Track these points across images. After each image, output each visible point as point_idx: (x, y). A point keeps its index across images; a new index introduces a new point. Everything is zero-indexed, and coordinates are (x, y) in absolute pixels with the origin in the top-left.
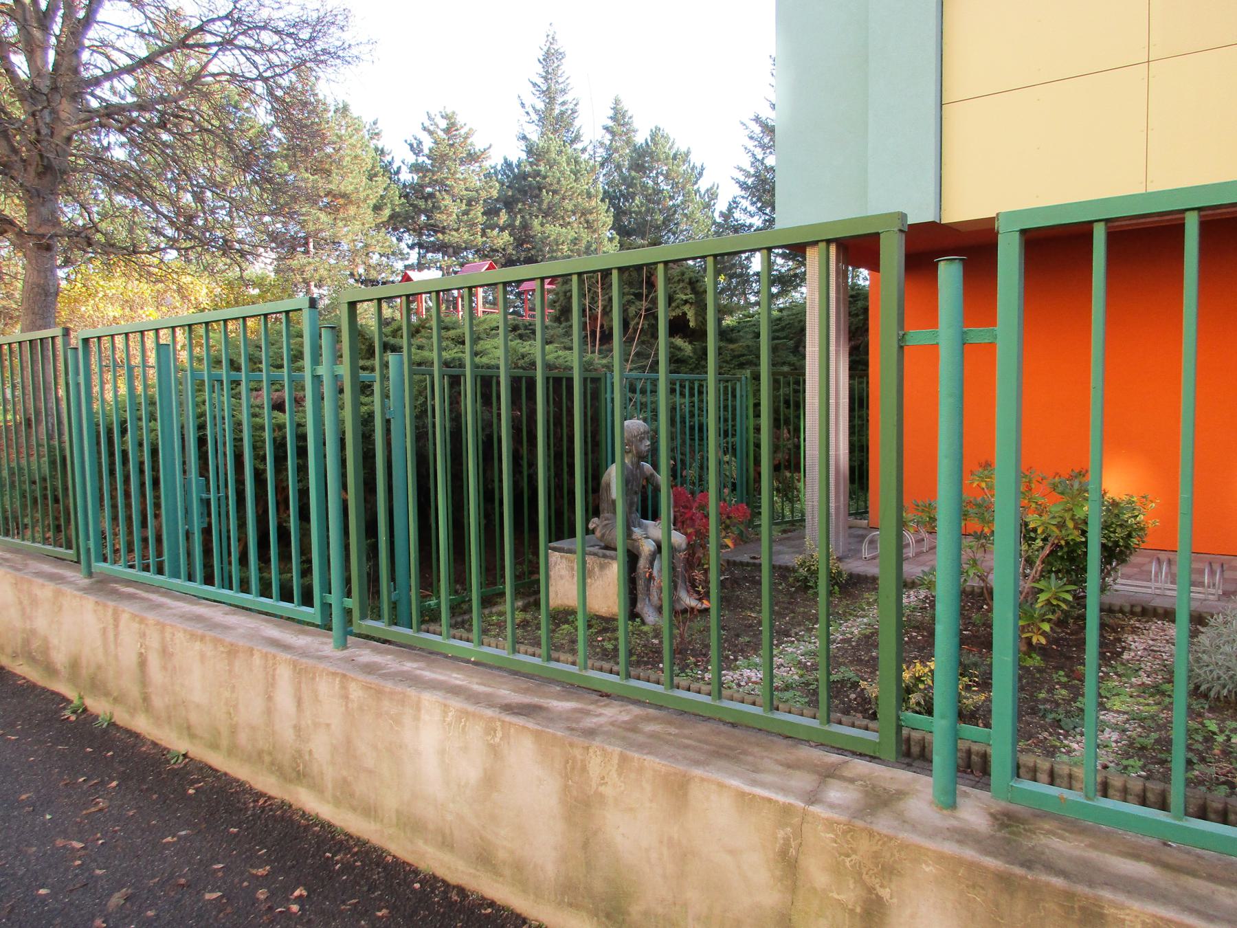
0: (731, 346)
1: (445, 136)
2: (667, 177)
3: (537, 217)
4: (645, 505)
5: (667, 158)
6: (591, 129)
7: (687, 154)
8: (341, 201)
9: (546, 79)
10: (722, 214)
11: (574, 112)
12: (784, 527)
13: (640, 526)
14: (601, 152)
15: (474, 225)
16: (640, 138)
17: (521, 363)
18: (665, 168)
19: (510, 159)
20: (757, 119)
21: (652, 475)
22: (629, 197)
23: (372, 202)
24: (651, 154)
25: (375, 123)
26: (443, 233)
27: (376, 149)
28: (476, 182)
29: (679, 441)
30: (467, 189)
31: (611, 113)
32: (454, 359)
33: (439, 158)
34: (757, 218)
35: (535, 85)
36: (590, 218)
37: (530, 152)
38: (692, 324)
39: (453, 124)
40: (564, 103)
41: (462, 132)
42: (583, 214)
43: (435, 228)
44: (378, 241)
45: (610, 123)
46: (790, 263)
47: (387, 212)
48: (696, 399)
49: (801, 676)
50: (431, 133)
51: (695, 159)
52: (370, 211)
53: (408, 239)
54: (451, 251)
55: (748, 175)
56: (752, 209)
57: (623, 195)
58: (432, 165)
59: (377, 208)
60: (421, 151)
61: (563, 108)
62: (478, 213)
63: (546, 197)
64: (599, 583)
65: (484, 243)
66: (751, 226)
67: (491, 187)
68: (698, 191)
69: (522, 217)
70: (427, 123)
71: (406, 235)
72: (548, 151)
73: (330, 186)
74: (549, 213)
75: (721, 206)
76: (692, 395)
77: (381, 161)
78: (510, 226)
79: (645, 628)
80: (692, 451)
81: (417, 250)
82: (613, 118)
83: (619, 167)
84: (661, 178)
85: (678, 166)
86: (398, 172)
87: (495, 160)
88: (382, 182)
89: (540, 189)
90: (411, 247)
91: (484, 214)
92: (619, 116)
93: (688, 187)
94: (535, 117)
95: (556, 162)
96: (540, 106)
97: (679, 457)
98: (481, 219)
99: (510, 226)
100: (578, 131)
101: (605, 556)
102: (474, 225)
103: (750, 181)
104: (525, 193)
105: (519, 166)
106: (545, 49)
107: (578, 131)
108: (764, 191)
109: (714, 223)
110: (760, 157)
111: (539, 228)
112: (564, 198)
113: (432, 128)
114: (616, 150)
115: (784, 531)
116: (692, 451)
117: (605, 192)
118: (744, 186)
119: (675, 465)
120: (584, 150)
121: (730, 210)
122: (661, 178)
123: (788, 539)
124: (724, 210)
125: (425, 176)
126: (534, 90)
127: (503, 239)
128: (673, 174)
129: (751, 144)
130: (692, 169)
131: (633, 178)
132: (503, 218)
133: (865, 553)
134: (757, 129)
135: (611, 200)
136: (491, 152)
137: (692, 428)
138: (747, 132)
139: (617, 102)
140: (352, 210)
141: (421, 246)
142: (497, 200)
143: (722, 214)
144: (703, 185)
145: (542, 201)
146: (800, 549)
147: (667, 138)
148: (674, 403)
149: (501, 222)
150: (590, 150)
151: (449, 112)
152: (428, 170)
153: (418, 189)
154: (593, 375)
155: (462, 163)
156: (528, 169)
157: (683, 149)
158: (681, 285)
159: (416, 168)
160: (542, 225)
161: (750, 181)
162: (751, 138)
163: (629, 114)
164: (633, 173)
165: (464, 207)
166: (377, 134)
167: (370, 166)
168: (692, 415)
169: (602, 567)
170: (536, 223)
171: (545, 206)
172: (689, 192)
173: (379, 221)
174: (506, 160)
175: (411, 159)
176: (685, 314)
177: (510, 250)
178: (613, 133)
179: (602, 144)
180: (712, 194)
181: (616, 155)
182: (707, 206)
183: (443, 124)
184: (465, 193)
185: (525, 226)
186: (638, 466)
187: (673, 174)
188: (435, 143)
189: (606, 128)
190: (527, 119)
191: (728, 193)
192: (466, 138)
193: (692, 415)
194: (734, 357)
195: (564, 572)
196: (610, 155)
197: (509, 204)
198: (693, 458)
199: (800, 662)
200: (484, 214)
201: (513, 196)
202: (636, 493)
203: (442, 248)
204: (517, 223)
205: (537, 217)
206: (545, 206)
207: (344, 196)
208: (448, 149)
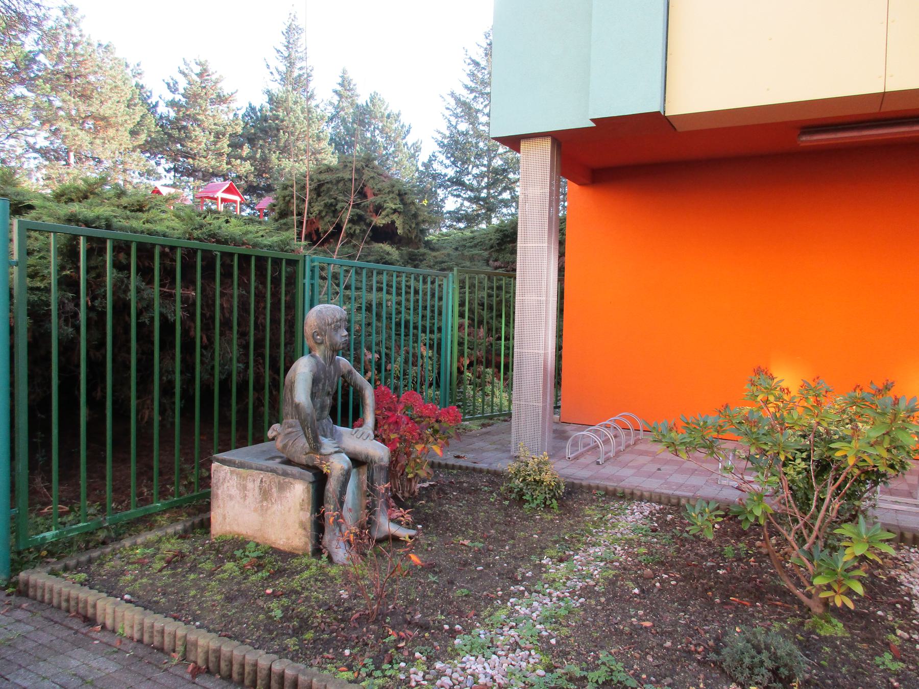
0: (434, 254)
1: (198, 80)
2: (382, 131)
3: (275, 152)
4: (344, 408)
5: (382, 117)
6: (323, 94)
7: (398, 115)
8: (102, 123)
9: (287, 47)
10: (424, 164)
11: (309, 76)
12: (483, 421)
13: (333, 435)
15: (221, 154)
16: (362, 101)
17: (196, 233)
18: (381, 124)
19: (254, 104)
21: (350, 372)
22: (351, 145)
25: (138, 65)
26: (194, 159)
27: (137, 85)
28: (225, 118)
29: (384, 336)
30: (215, 124)
31: (340, 80)
32: (98, 218)
33: (192, 97)
34: (450, 169)
35: (278, 51)
36: (319, 156)
37: (271, 101)
38: (399, 231)
39: (205, 70)
40: (301, 69)
42: (313, 153)
44: (134, 160)
45: (339, 88)
46: (474, 206)
47: (143, 137)
48: (403, 298)
49: (550, 669)
50: (185, 75)
52: (127, 134)
53: (166, 164)
54: (200, 174)
55: (444, 137)
56: (448, 162)
59: (134, 133)
60: (176, 90)
61: (301, 72)
63: (283, 136)
64: (277, 507)
66: (445, 175)
67: (236, 125)
68: (406, 144)
69: (263, 152)
70: (183, 68)
72: (286, 100)
74: (284, 150)
75: (423, 157)
78: (251, 158)
79: (333, 571)
80: (398, 347)
81: (173, 173)
84: (377, 132)
85: (391, 124)
87: (240, 105)
88: (140, 110)
89: (278, 130)
90: (168, 171)
91: (229, 146)
92: (345, 83)
93: (399, 140)
94: (278, 77)
95: (292, 110)
96: (283, 68)
97: (383, 351)
98: (227, 150)
99: (251, 158)
100: (313, 91)
101: (285, 474)
103: (446, 141)
105: (261, 110)
106: (288, 24)
107: (313, 91)
108: (456, 149)
109: (417, 170)
110: (454, 124)
111: (276, 161)
113: (186, 72)
114: (343, 109)
115: (483, 425)
116: (398, 347)
120: (317, 106)
121: (430, 161)
122: (377, 132)
123: (487, 433)
124: (426, 161)
125: (179, 111)
126: (277, 55)
127: (246, 167)
128: (387, 130)
130: (402, 127)
131: (355, 130)
132: (246, 150)
133: (568, 453)
134: (453, 102)
137: (398, 324)
138: (445, 103)
139: (344, 72)
140: (111, 132)
141: (176, 170)
143: (424, 164)
144: (410, 140)
146: (505, 447)
147: (382, 101)
148: (381, 298)
149: (244, 154)
151: (203, 61)
152: (182, 106)
153: (175, 123)
155: (213, 103)
156: (269, 114)
157: (396, 112)
158: (391, 195)
159: (172, 104)
160: (278, 158)
161: (446, 141)
162: (448, 109)
163: (353, 82)
164: (355, 126)
165: (212, 139)
166: (139, 74)
167: (129, 97)
168: (399, 312)
169: (282, 488)
170: (274, 157)
171: (282, 144)
172: (399, 144)
173: (136, 144)
174: (250, 104)
175: (169, 96)
176: (393, 222)
177: (251, 178)
179: (331, 103)
180: (417, 148)
181: (342, 113)
182: (413, 156)
183: (198, 69)
184: (214, 127)
185: (265, 159)
186: (332, 361)
187: (387, 130)
188: (189, 83)
189: (336, 92)
190: (272, 78)
191: (429, 149)
193: (399, 312)
194: (437, 263)
195: (234, 491)
196: (338, 113)
197: (252, 140)
198: (398, 352)
200: (229, 146)
201: (255, 134)
203: (191, 172)
204: (258, 156)
205: (275, 152)
206: (282, 144)
207: (104, 118)
208: (199, 93)
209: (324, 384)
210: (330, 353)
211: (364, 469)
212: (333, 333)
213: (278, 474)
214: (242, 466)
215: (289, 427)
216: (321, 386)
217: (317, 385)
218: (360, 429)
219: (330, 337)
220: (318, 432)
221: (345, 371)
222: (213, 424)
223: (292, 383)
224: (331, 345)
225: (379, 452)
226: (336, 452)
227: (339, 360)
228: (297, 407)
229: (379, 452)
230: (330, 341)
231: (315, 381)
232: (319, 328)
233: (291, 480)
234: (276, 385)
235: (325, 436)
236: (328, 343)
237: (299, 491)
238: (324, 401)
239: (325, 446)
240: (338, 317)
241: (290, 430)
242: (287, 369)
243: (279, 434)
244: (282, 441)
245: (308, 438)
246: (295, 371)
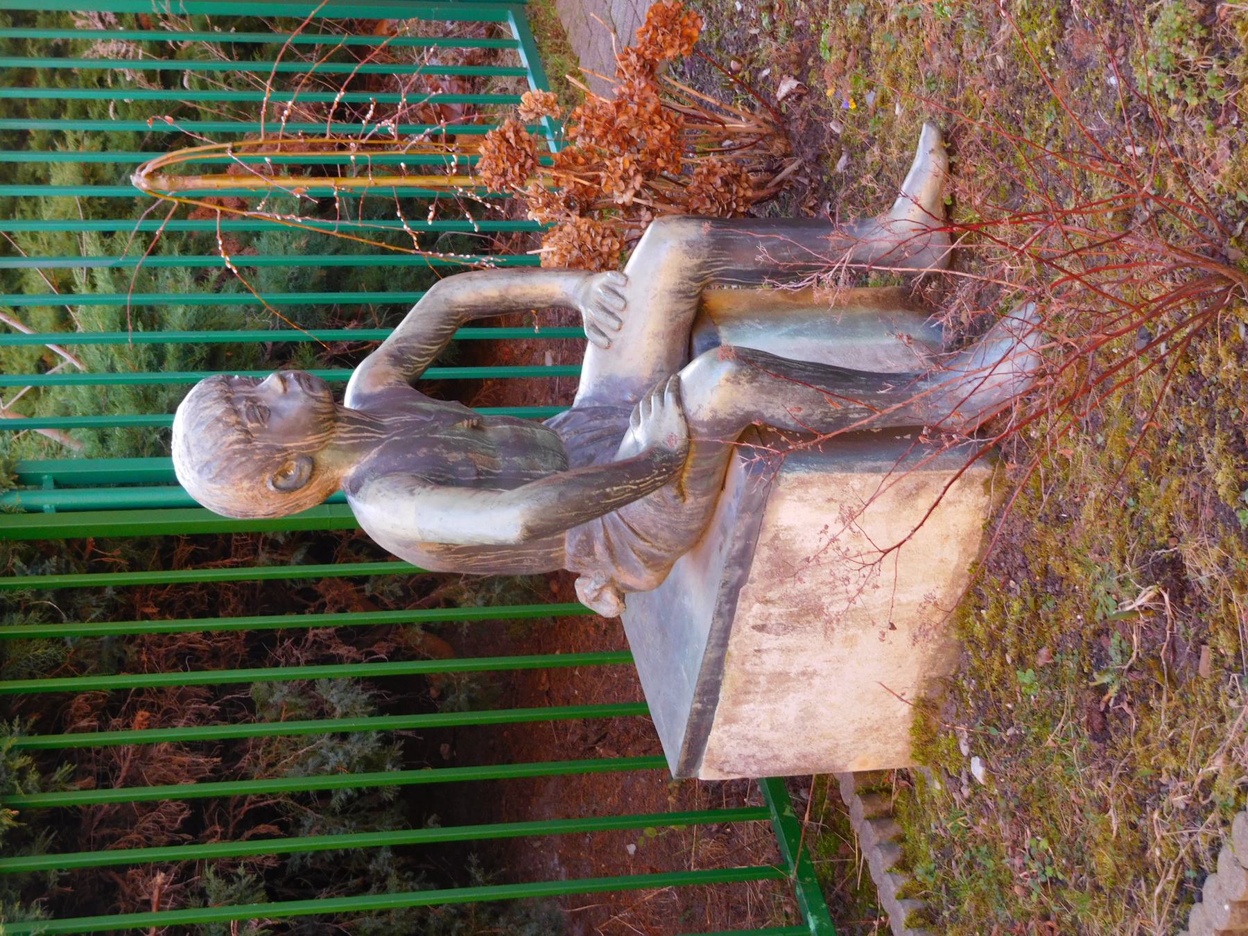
4: (493, 380)
13: (614, 412)
21: (397, 358)
186: (366, 421)
195: (790, 707)
209: (448, 445)
210: (342, 431)
211: (723, 298)
212: (276, 422)
213: (741, 582)
214: (709, 692)
215: (591, 553)
216: (455, 457)
217: (452, 469)
218: (587, 314)
219: (290, 432)
220: (603, 460)
221: (395, 376)
222: (520, 725)
223: (449, 549)
224: (317, 427)
225: (662, 256)
226: (679, 400)
227: (358, 398)
228: (534, 534)
229: (662, 256)
230: (303, 432)
231: (440, 477)
232: (261, 471)
233: (764, 538)
234: (421, 586)
235: (618, 435)
236: (311, 439)
237: (804, 510)
238: (504, 444)
239: (661, 437)
240: (219, 410)
241: (599, 548)
242: (380, 554)
243: (611, 582)
244: (634, 571)
245: (637, 494)
246: (409, 544)
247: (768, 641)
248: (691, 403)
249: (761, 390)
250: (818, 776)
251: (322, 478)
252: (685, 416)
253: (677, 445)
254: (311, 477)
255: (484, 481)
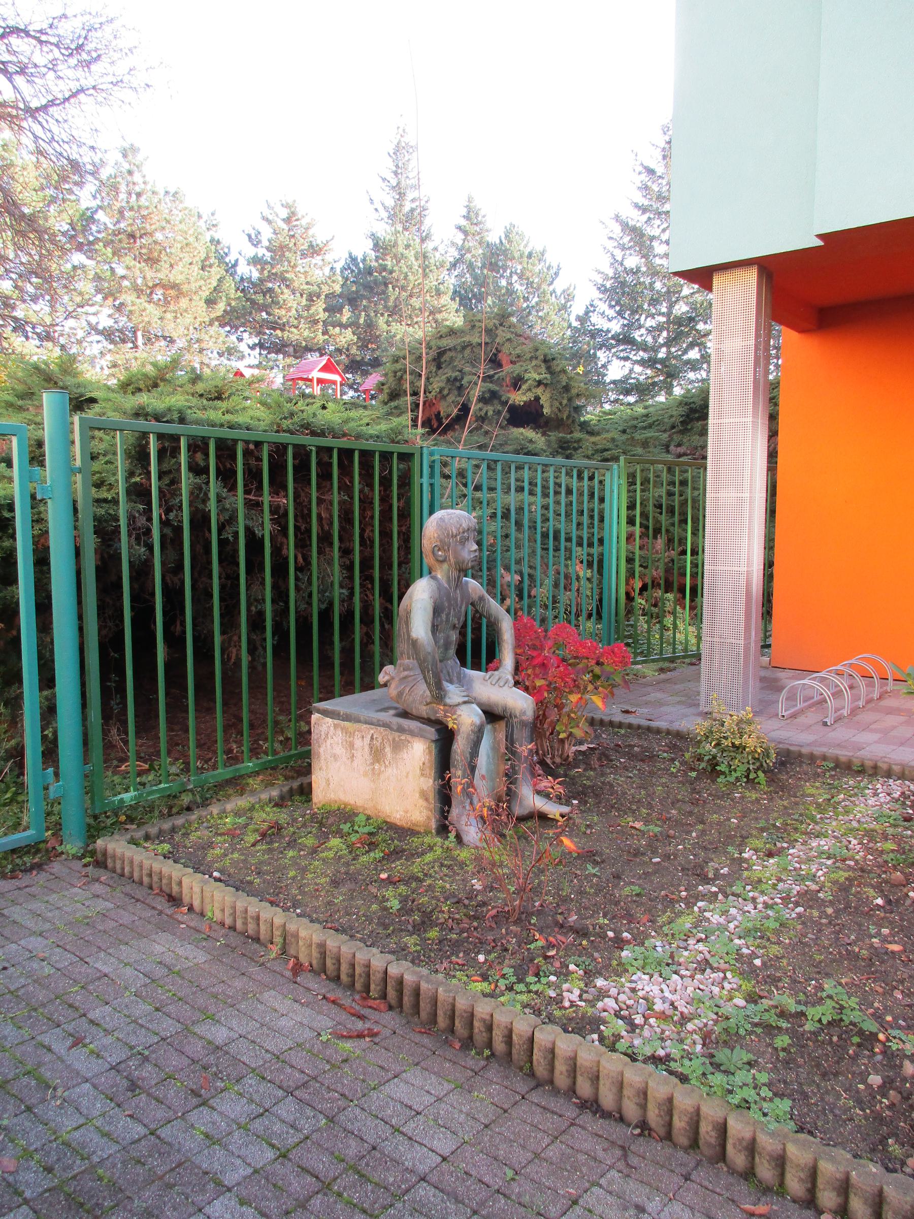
0: (593, 439)
3: (382, 315)
5: (521, 257)
6: (443, 234)
9: (396, 173)
10: (578, 318)
13: (460, 681)
14: (453, 254)
15: (316, 322)
16: (493, 237)
17: (286, 424)
18: (519, 267)
19: (355, 253)
20: (617, 218)
21: (481, 598)
22: (480, 298)
23: (205, 294)
24: (505, 252)
25: (213, 214)
26: (282, 330)
30: (307, 283)
31: (464, 212)
33: (279, 251)
34: (615, 321)
35: (384, 180)
38: (546, 411)
39: (294, 214)
41: (304, 222)
42: (431, 313)
43: (275, 326)
45: (463, 222)
46: (649, 372)
47: (221, 307)
49: (753, 999)
50: (269, 222)
51: (551, 258)
54: (291, 350)
55: (607, 278)
56: (611, 313)
57: (474, 296)
58: (272, 258)
60: (259, 242)
61: (414, 205)
62: (319, 308)
63: (393, 293)
64: (391, 772)
65: (326, 342)
67: (334, 282)
70: (267, 213)
71: (246, 335)
72: (395, 245)
73: (159, 275)
74: (394, 311)
75: (578, 309)
76: (545, 495)
77: (217, 251)
78: (353, 324)
79: (464, 855)
81: (258, 350)
82: (467, 217)
83: (471, 266)
84: (515, 278)
85: (533, 265)
86: (235, 265)
88: (216, 272)
89: (386, 285)
90: (252, 348)
92: (471, 215)
93: (544, 286)
94: (385, 215)
96: (390, 203)
97: (526, 570)
98: (323, 316)
99: (353, 324)
100: (429, 230)
101: (401, 730)
102: (316, 322)
103: (608, 284)
104: (372, 289)
105: (364, 260)
107: (429, 230)
108: (623, 294)
110: (620, 259)
111: (385, 326)
112: (411, 296)
113: (270, 217)
115: (662, 670)
117: (455, 292)
118: (602, 289)
119: (521, 582)
120: (436, 249)
122: (515, 278)
125: (263, 269)
126: (383, 185)
127: (347, 337)
128: (528, 274)
129: (611, 245)
130: (548, 269)
132: (346, 315)
134: (617, 229)
135: (461, 300)
136: (332, 245)
137: (545, 536)
140: (184, 303)
141: (261, 345)
142: (340, 296)
144: (559, 285)
145: (388, 297)
146: (691, 700)
147: (521, 236)
148: (522, 501)
149: (344, 320)
150: (441, 249)
151: (290, 202)
152: (266, 263)
154: (404, 449)
155: (304, 256)
156: (374, 264)
157: (539, 248)
159: (255, 261)
160: (388, 323)
161: (608, 284)
163: (481, 213)
167: (203, 256)
168: (546, 520)
169: (397, 747)
170: (381, 321)
171: (391, 304)
172: (544, 292)
173: (213, 316)
174: (350, 255)
175: (251, 251)
176: (537, 399)
177: (354, 350)
178: (466, 233)
180: (569, 296)
181: (468, 256)
182: (564, 308)
183: (284, 213)
184: (306, 287)
185: (370, 325)
186: (458, 584)
188: (275, 233)
189: (459, 228)
190: (376, 215)
192: (307, 229)
193: (546, 520)
194: (597, 451)
195: (339, 750)
196: (462, 256)
197: (353, 301)
198: (545, 573)
199: (740, 957)
200: (325, 310)
201: (357, 292)
202: (454, 627)
203: (280, 348)
205: (382, 315)
206: (391, 304)
207: (174, 286)
209: (448, 615)
210: (456, 574)
212: (460, 547)
213: (391, 729)
214: (347, 718)
216: (444, 616)
217: (439, 615)
219: (456, 553)
221: (475, 597)
223: (408, 613)
224: (457, 563)
226: (465, 702)
227: (467, 582)
228: (414, 643)
229: (520, 703)
230: (455, 557)
231: (437, 610)
233: (409, 737)
235: (451, 682)
236: (452, 560)
237: (419, 751)
238: (448, 637)
239: (450, 695)
240: (465, 525)
241: (406, 673)
242: (400, 598)
243: (393, 678)
244: (397, 687)
246: (411, 598)
247: (367, 740)
248: (464, 707)
249: (468, 735)
250: (352, 692)
251: (437, 565)
252: (459, 704)
253: (448, 701)
254: (437, 560)
255: (435, 629)
